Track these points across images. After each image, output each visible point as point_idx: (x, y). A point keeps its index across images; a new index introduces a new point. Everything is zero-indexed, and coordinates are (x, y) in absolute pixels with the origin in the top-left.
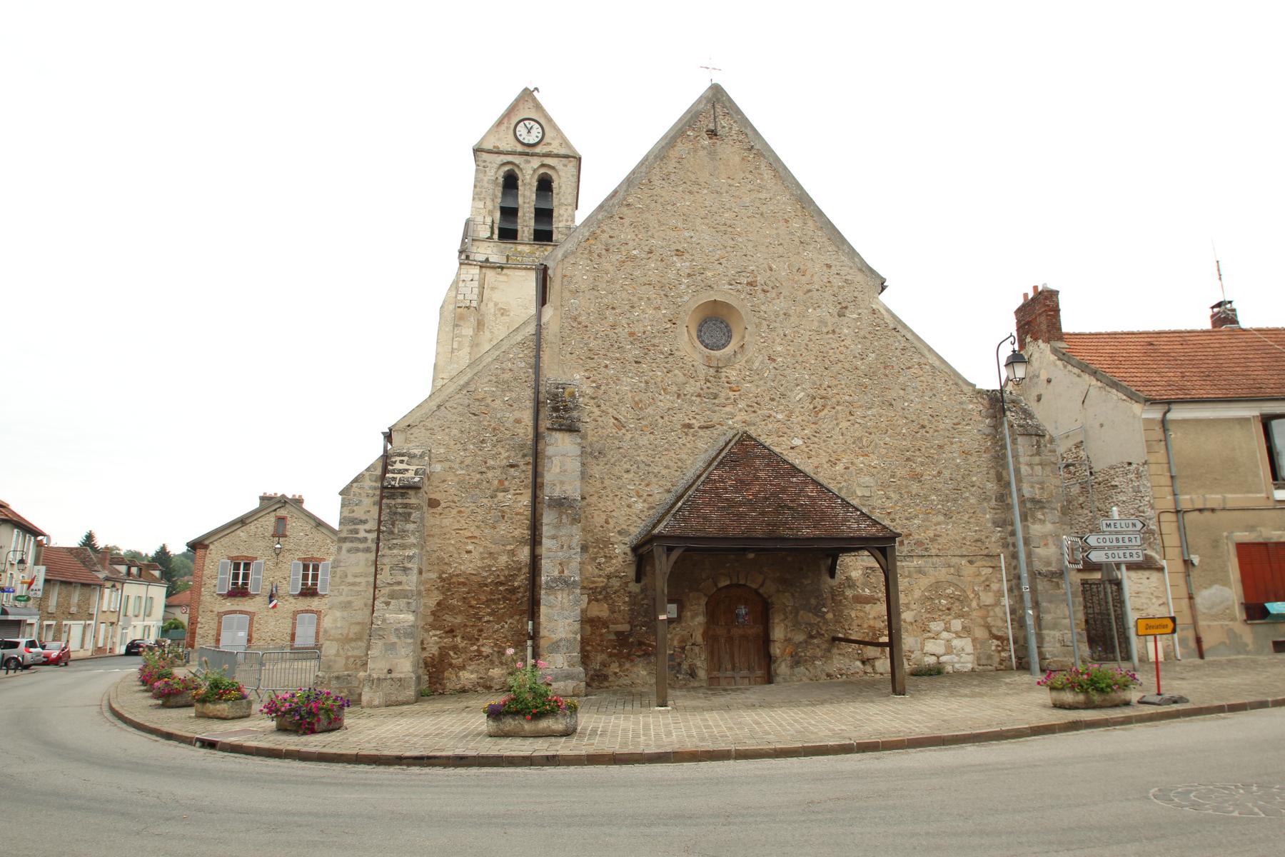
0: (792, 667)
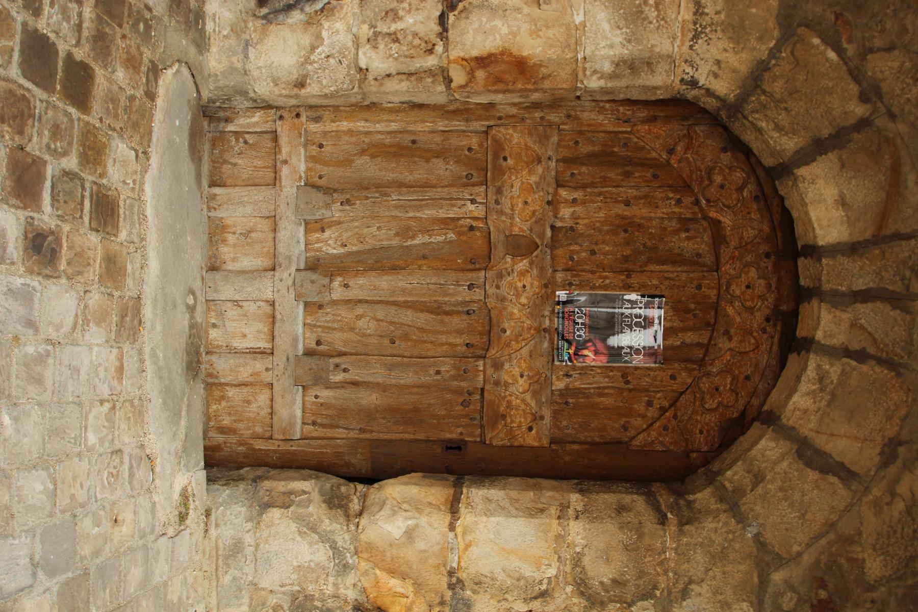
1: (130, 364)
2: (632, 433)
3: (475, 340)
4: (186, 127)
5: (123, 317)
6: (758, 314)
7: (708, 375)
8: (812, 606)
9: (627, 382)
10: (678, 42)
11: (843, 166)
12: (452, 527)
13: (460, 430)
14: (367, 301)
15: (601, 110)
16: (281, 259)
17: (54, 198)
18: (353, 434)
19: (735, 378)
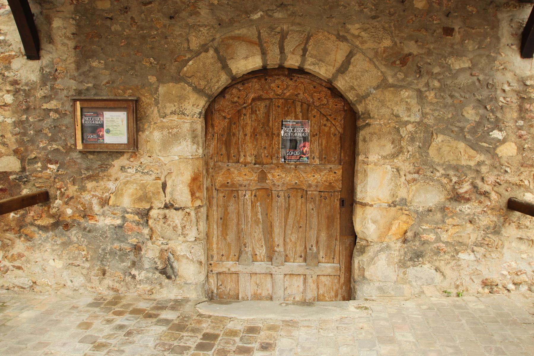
0: (402, 264)
1: (306, 324)
2: (337, 132)
3: (300, 194)
4: (219, 305)
5: (289, 325)
6: (289, 83)
7: (313, 103)
8: (403, 66)
9: (316, 134)
10: (186, 121)
11: (232, 58)
12: (371, 206)
13: (336, 201)
14: (284, 237)
15: (209, 146)
16: (268, 271)
17: (250, 343)
18: (338, 243)
19: (315, 92)
